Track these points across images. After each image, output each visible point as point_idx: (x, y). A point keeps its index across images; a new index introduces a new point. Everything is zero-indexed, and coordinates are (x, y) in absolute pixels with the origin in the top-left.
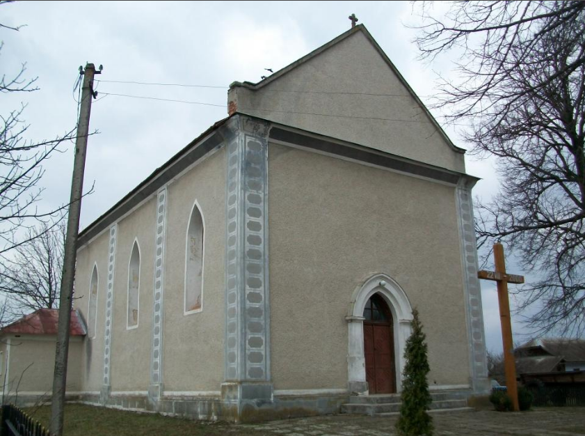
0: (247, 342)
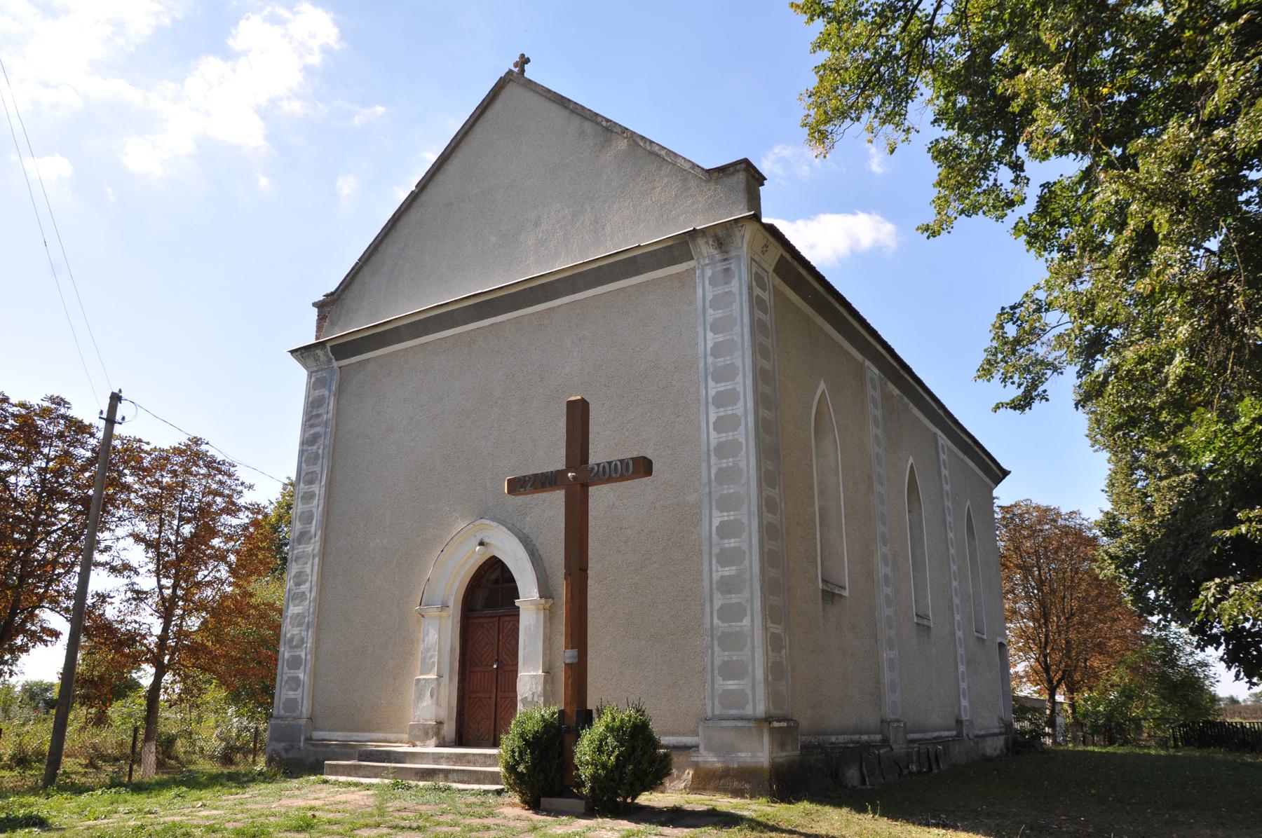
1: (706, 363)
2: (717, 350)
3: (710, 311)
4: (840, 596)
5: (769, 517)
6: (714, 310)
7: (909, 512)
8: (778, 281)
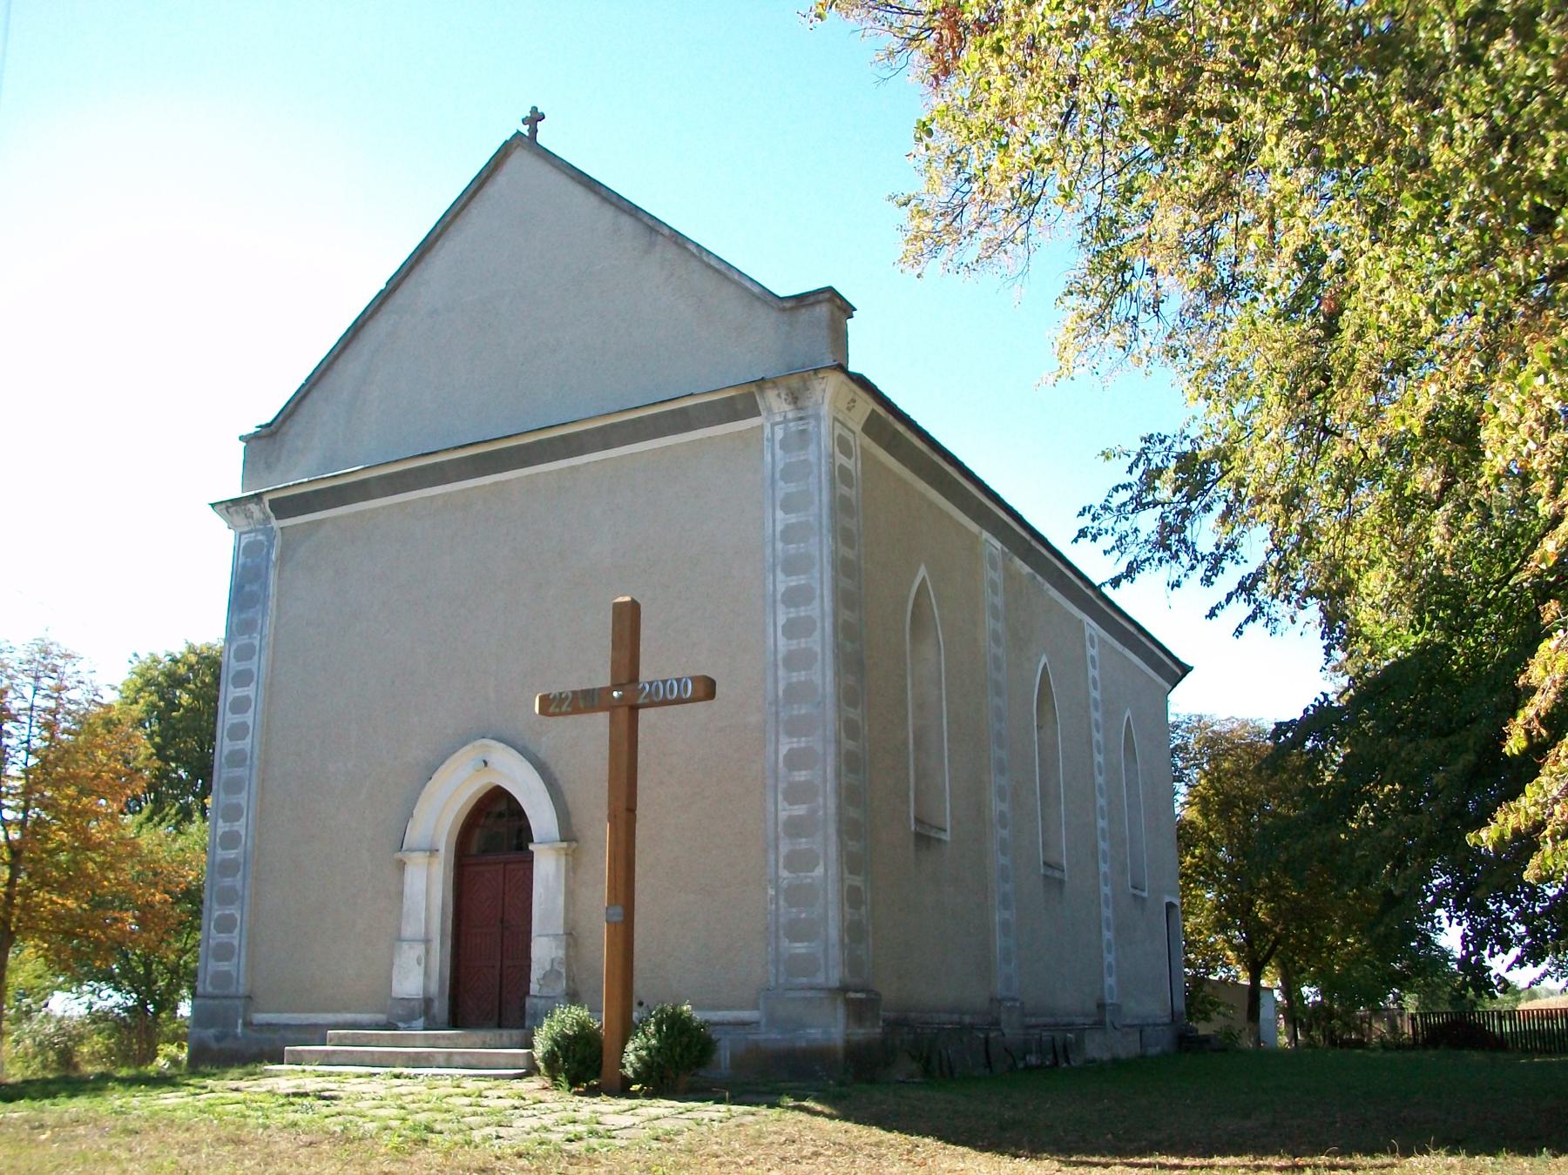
0: (212, 924)
1: (774, 549)
2: (788, 534)
3: (781, 484)
4: (939, 840)
5: (850, 744)
6: (790, 941)
7: (1040, 727)
8: (867, 441)
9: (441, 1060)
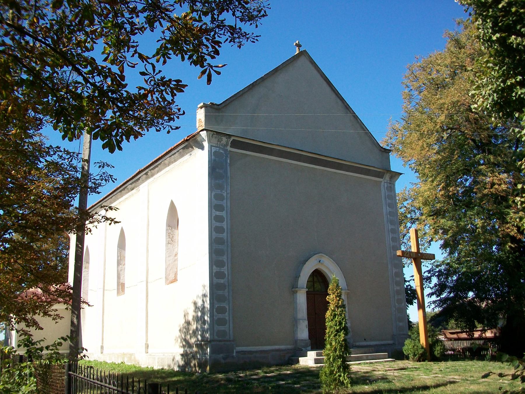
0: (215, 310)
9: (365, 358)
